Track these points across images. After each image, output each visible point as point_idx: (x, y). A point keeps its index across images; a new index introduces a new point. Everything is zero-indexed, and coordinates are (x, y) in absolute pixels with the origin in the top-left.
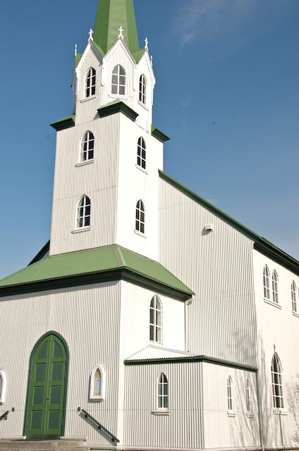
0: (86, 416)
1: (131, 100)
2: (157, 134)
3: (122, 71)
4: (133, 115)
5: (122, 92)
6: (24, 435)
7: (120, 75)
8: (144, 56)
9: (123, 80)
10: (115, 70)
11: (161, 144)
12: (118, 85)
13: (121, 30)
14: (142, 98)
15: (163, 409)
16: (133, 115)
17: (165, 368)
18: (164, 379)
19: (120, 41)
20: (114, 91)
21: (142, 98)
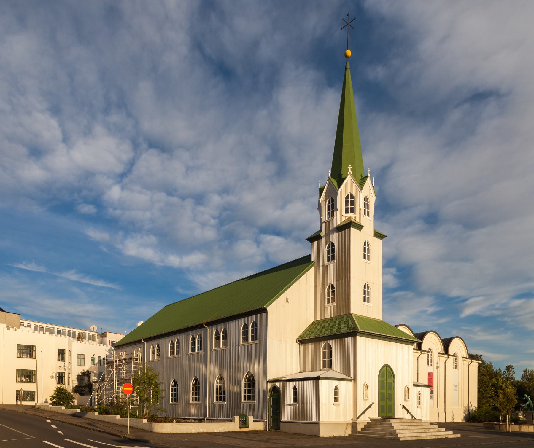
0: (404, 407)
1: (356, 217)
2: (378, 235)
3: (352, 197)
4: (359, 227)
5: (353, 211)
6: (379, 416)
7: (350, 201)
8: (367, 182)
9: (353, 203)
10: (347, 197)
11: (380, 241)
12: (350, 207)
13: (350, 168)
14: (367, 213)
15: (295, 403)
16: (359, 227)
17: (295, 383)
18: (336, 388)
19: (349, 176)
20: (347, 212)
21: (367, 213)
